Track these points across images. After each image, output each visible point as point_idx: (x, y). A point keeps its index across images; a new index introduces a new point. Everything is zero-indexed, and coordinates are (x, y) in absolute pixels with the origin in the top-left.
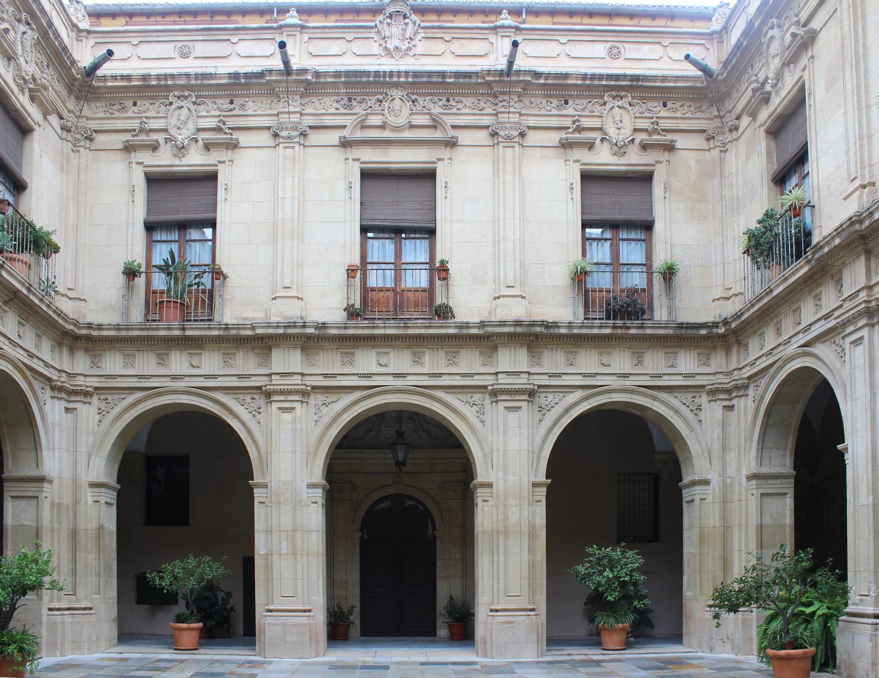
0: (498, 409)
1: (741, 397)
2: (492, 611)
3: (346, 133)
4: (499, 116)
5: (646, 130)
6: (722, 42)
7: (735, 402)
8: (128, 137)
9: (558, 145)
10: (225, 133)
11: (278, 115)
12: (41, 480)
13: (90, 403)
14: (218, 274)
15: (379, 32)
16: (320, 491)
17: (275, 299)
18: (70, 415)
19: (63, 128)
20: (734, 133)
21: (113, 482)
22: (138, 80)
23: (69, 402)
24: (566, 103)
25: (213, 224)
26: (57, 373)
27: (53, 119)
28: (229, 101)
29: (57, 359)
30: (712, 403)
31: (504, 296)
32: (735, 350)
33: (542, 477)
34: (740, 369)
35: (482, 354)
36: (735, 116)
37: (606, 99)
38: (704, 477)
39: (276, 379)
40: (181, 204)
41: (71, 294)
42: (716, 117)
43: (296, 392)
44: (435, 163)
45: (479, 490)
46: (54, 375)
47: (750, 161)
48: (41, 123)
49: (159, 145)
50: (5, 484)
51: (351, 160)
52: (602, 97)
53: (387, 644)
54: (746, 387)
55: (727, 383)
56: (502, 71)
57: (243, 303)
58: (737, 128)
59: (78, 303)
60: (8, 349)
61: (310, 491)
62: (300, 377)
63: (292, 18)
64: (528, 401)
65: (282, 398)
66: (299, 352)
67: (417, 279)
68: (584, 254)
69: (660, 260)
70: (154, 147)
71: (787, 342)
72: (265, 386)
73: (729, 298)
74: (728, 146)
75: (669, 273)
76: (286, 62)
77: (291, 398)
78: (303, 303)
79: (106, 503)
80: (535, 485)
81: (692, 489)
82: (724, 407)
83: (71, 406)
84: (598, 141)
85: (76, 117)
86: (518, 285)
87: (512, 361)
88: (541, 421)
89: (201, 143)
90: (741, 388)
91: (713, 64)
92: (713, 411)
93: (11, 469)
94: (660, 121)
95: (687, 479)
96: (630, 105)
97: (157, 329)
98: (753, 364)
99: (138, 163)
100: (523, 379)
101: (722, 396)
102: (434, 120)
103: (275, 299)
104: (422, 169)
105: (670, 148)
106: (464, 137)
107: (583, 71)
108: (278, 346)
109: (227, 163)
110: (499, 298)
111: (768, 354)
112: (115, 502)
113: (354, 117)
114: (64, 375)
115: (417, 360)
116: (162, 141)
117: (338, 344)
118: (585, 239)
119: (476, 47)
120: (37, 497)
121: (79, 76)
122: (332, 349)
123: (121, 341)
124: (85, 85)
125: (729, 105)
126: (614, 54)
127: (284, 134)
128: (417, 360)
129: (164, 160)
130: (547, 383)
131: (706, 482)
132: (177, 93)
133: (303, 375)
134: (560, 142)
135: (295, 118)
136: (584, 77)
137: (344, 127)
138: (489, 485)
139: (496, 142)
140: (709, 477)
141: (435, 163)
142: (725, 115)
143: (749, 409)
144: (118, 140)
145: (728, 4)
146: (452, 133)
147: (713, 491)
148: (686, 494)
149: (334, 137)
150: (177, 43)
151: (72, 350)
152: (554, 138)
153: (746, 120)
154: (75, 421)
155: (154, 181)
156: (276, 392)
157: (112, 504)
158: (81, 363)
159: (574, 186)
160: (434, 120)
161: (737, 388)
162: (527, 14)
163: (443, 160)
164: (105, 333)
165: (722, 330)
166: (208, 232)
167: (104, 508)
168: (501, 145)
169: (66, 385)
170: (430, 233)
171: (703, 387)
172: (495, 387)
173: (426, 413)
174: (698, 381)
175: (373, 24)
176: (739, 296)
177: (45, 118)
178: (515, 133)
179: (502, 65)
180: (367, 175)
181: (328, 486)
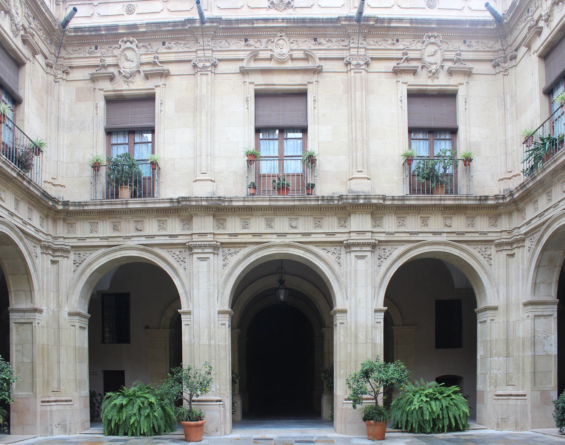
1: (519, 247)
2: (497, 395)
3: (244, 64)
4: (351, 50)
7: (515, 251)
8: (93, 71)
9: (391, 71)
12: (35, 310)
13: (68, 257)
14: (154, 165)
16: (228, 316)
17: (195, 181)
18: (55, 266)
21: (85, 311)
22: (345, 20)
23: (54, 256)
24: (397, 41)
25: (152, 130)
27: (39, 57)
28: (161, 44)
29: (45, 228)
30: (499, 253)
31: (355, 178)
33: (380, 304)
34: (519, 228)
35: (490, 218)
36: (514, 48)
37: (120, 43)
39: (196, 238)
40: (130, 116)
41: (55, 182)
42: (500, 50)
43: (210, 246)
44: (306, 85)
45: (338, 315)
46: (40, 236)
49: (115, 76)
52: (117, 42)
54: (523, 240)
58: (515, 57)
59: (59, 188)
60: (8, 218)
61: (221, 316)
65: (200, 251)
67: (294, 167)
69: (462, 151)
72: (188, 243)
73: (510, 179)
75: (468, 161)
76: (201, 14)
77: (364, 249)
80: (376, 311)
81: (485, 313)
82: (507, 255)
83: (56, 259)
84: (420, 68)
86: (365, 170)
87: (204, 225)
88: (379, 266)
89: (142, 73)
92: (499, 258)
95: (481, 305)
97: (115, 204)
99: (99, 90)
100: (368, 236)
101: (506, 248)
102: (307, 55)
103: (195, 181)
104: (299, 90)
106: (326, 66)
108: (355, 213)
110: (352, 179)
112: (87, 327)
113: (248, 53)
115: (425, 222)
116: (116, 73)
117: (273, 212)
118: (410, 139)
120: (32, 323)
121: (57, 28)
125: (510, 39)
127: (200, 65)
128: (425, 222)
131: (495, 308)
132: (125, 39)
133: (214, 234)
134: (393, 70)
136: (411, 21)
137: (242, 60)
138: (344, 312)
139: (349, 69)
140: (42, 308)
141: (306, 85)
142: (507, 48)
143: (526, 257)
144: (85, 74)
146: (318, 63)
149: (235, 67)
151: (55, 221)
153: (523, 49)
155: (113, 101)
156: (196, 247)
157: (85, 328)
158: (61, 230)
160: (307, 55)
161: (517, 241)
163: (160, 86)
165: (60, 207)
166: (149, 137)
167: (78, 330)
168: (352, 71)
171: (492, 241)
172: (349, 241)
174: (489, 237)
177: (34, 57)
179: (354, 13)
180: (259, 95)
181: (233, 312)
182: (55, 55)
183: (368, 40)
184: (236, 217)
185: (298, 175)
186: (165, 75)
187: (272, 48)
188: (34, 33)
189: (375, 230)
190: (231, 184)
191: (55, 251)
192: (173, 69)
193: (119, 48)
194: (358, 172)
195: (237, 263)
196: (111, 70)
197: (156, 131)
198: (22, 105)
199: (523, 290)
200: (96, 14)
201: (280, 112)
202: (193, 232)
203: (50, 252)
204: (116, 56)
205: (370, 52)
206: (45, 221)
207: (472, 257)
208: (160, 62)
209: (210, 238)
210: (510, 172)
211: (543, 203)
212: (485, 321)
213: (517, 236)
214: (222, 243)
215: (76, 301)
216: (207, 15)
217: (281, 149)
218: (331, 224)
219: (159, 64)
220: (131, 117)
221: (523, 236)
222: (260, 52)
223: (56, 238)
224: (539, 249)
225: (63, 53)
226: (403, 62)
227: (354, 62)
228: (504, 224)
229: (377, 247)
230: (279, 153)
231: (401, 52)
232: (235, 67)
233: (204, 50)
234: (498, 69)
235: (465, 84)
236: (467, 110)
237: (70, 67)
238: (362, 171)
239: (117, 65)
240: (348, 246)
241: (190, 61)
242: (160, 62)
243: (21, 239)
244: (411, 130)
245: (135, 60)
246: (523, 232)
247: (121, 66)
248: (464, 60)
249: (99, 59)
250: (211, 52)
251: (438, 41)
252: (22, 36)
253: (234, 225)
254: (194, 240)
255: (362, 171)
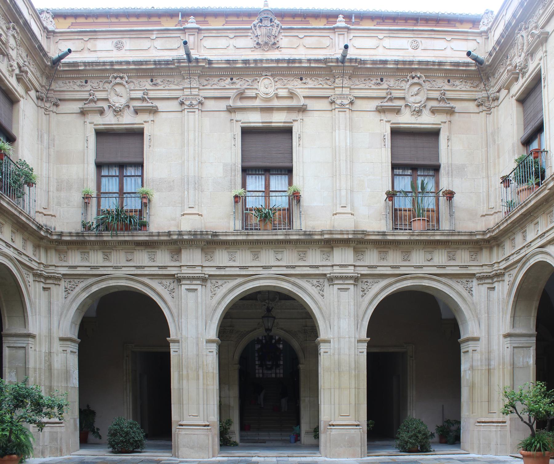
0: (333, 290)
2: (479, 422)
3: (231, 103)
5: (437, 99)
6: (488, 38)
7: (496, 285)
8: (80, 105)
10: (148, 102)
11: (183, 90)
15: (253, 33)
17: (183, 215)
18: (47, 292)
19: (38, 98)
20: (496, 101)
21: (75, 336)
23: (45, 284)
26: (36, 264)
29: (37, 255)
30: (480, 285)
32: (495, 250)
33: (363, 335)
34: (499, 263)
38: (475, 335)
40: (121, 151)
41: (45, 212)
43: (198, 278)
45: (321, 344)
46: (34, 265)
47: (508, 121)
48: (24, 96)
49: (104, 110)
50: (4, 338)
51: (234, 121)
53: (379, 441)
54: (503, 274)
55: (490, 272)
56: (337, 59)
57: (163, 218)
61: (208, 344)
62: (200, 268)
63: (341, 22)
64: (354, 285)
65: (341, 282)
66: (200, 251)
67: (280, 201)
68: (244, 185)
70: (398, 111)
71: (529, 245)
72: (177, 274)
74: (492, 110)
75: (450, 195)
76: (188, 54)
77: (195, 282)
78: (202, 218)
79: (71, 352)
82: (488, 288)
84: (403, 107)
85: (47, 90)
88: (363, 296)
90: (499, 276)
91: (482, 55)
93: (8, 328)
94: (447, 93)
95: (463, 337)
96: (126, 82)
98: (507, 259)
101: (487, 281)
103: (183, 215)
105: (451, 112)
106: (311, 104)
107: (397, 58)
109: (299, 121)
110: (336, 214)
111: (518, 252)
112: (77, 351)
113: (235, 91)
114: (42, 266)
115: (256, 257)
118: (393, 175)
119: (326, 42)
120: (24, 347)
122: (139, 250)
123: (78, 243)
124: (54, 69)
126: (119, 47)
128: (256, 257)
129: (109, 120)
130: (239, 273)
131: (476, 339)
134: (376, 108)
135: (195, 92)
137: (229, 98)
138: (328, 341)
139: (333, 108)
143: (504, 291)
144: (76, 107)
145: (492, 12)
146: (302, 102)
147: (481, 346)
148: (463, 347)
150: (113, 40)
151: (47, 250)
152: (375, 104)
153: (504, 92)
154: (50, 296)
157: (75, 352)
158: (53, 259)
159: (386, 137)
160: (291, 93)
161: (497, 275)
162: (355, 17)
163: (148, 122)
164: (162, 238)
168: (186, 111)
169: (43, 273)
170: (288, 171)
172: (332, 275)
173: (248, 293)
175: (250, 27)
176: (499, 213)
177: (27, 92)
178: (346, 102)
182: (45, 88)
183: (353, 79)
184: (223, 250)
185: (284, 210)
186: (154, 111)
187: (257, 87)
188: (28, 70)
189: (357, 264)
190: (219, 217)
191: (48, 279)
192: (161, 105)
193: (109, 83)
194: (342, 207)
195: (225, 294)
196: (101, 104)
197: (145, 165)
198: (16, 142)
199: (502, 322)
200: (86, 49)
201: (267, 152)
202: (181, 264)
203: (43, 280)
204: (107, 91)
205: (355, 91)
206: (37, 250)
207: (452, 290)
208: (150, 99)
209: (198, 270)
210: (493, 208)
211: (519, 242)
212: (468, 351)
213: (497, 270)
214: (210, 275)
215: (66, 324)
216: (194, 54)
217: (267, 185)
218: (315, 257)
219: (148, 100)
220: (120, 151)
221: (503, 271)
222: (246, 91)
223: (46, 266)
224: (85, 295)
225: (54, 86)
226: (387, 101)
227: (338, 102)
228: (485, 258)
229: (360, 281)
230: (265, 188)
231: (385, 91)
232: (223, 105)
233: (191, 88)
234: (481, 108)
235: (447, 122)
236: (450, 148)
237: (60, 100)
238: (345, 207)
239: (107, 100)
240: (331, 280)
241: (177, 98)
242: (148, 98)
243: (18, 270)
244: (394, 167)
245: (124, 95)
246: (502, 267)
247: (111, 100)
248: (448, 99)
249: (88, 93)
250: (197, 90)
251: (421, 81)
252: (16, 75)
253: (222, 258)
254: (183, 272)
255: (345, 207)
